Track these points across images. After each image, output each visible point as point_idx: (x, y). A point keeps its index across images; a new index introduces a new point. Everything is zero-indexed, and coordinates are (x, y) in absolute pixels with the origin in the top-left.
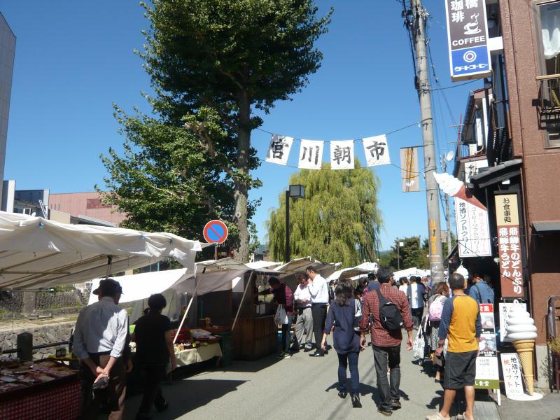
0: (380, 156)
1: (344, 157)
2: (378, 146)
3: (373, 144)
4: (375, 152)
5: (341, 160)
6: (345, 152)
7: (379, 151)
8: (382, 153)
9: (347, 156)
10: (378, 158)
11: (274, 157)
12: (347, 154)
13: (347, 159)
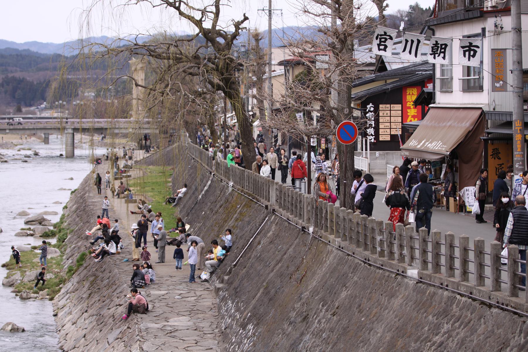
0: (471, 58)
1: (441, 52)
2: (472, 48)
3: (468, 44)
4: (467, 53)
5: (437, 55)
6: (441, 49)
7: (472, 53)
8: (474, 56)
9: (442, 52)
10: (469, 60)
11: (379, 50)
12: (443, 50)
13: (442, 55)
